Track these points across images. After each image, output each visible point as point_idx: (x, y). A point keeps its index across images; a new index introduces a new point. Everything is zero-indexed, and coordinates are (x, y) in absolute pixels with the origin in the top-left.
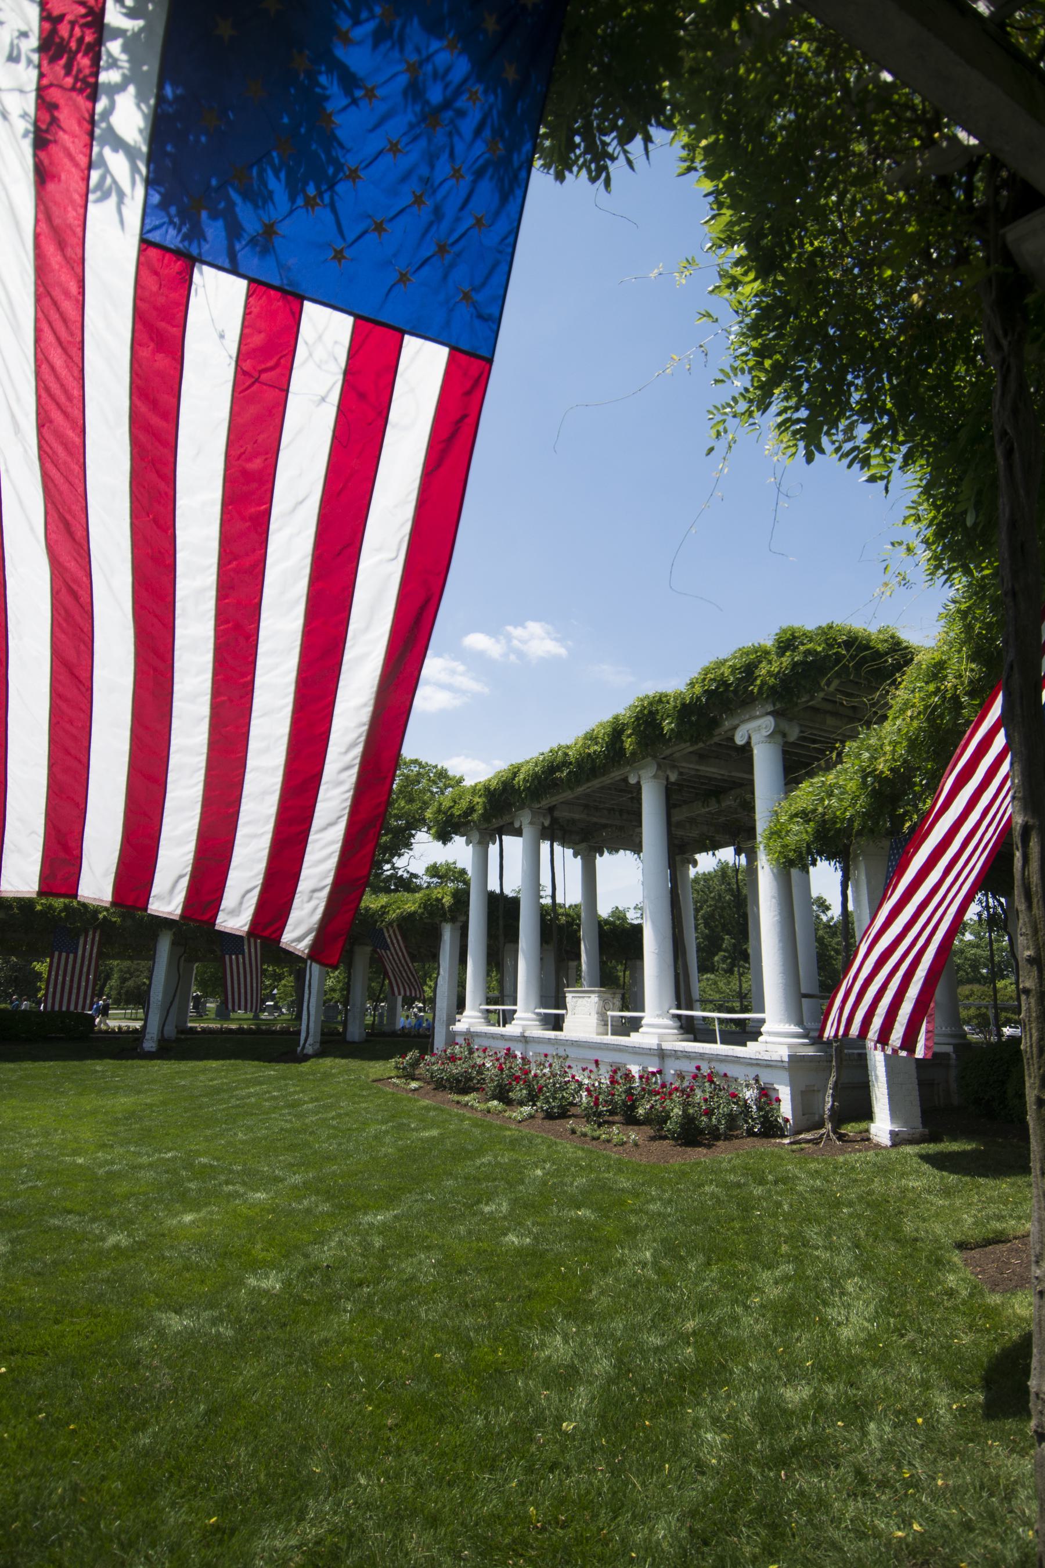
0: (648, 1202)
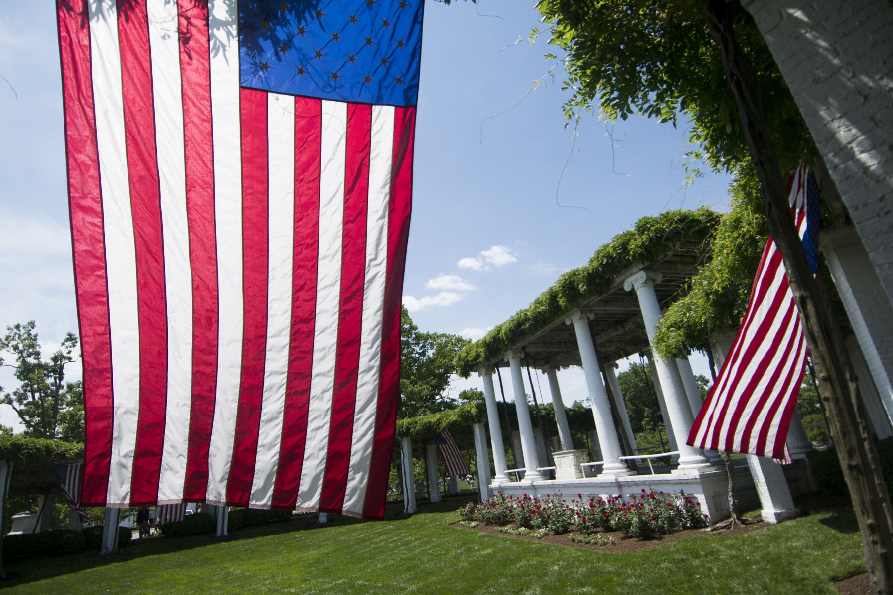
0: (626, 578)
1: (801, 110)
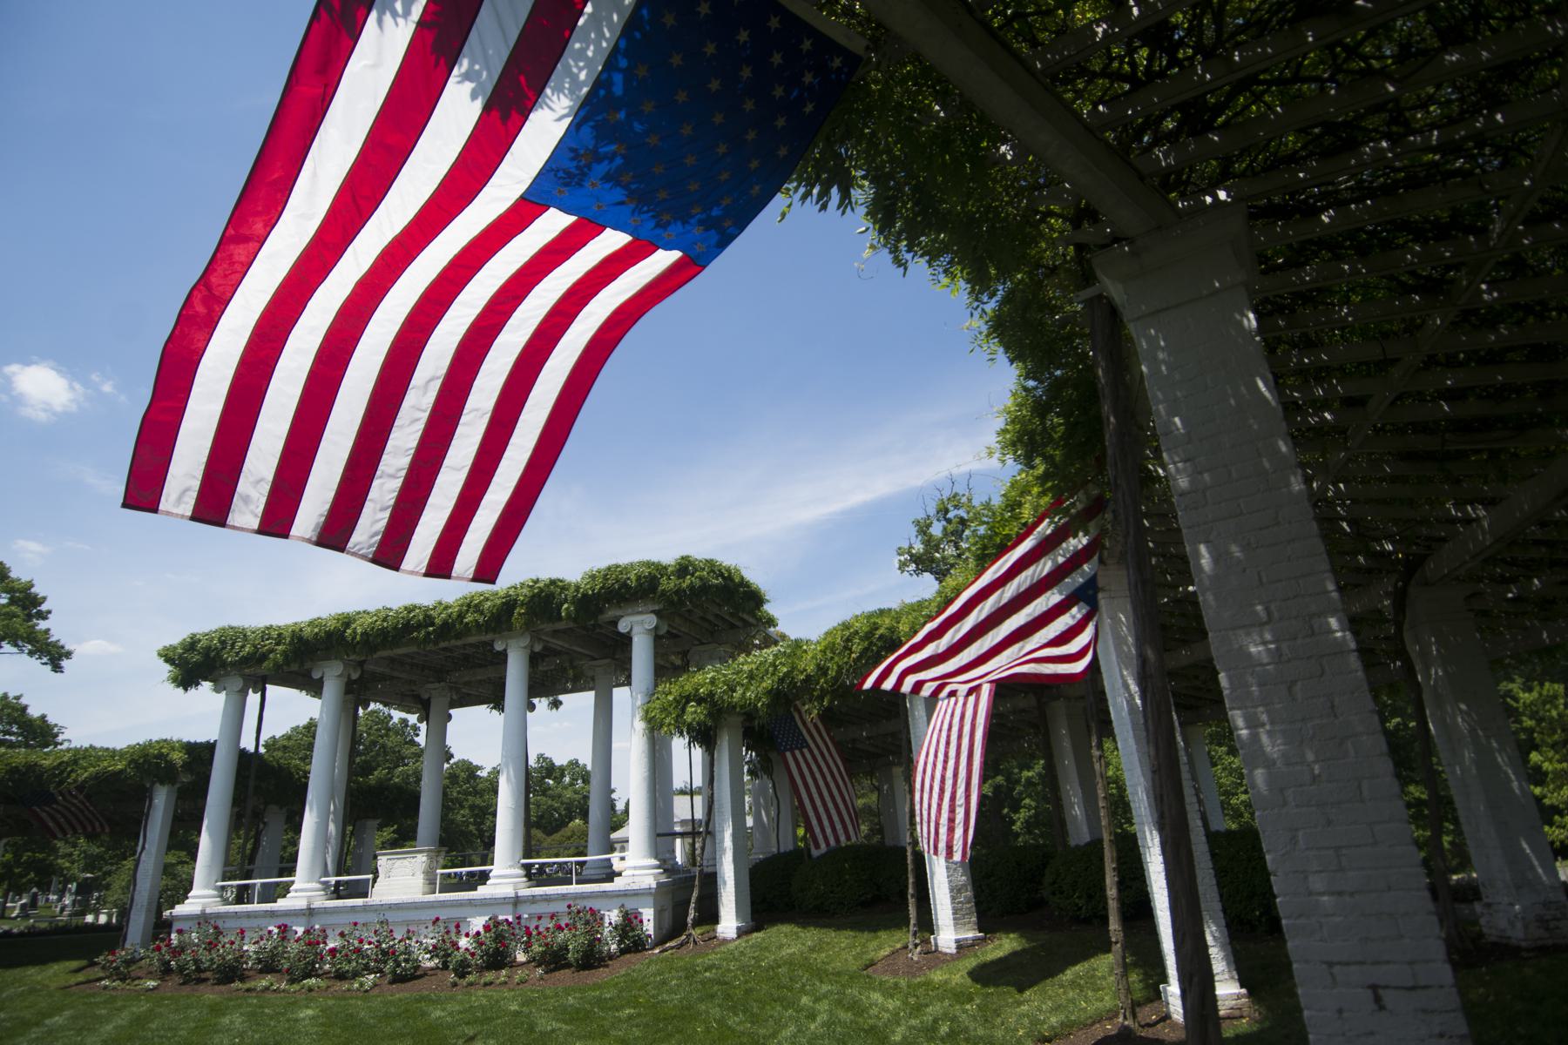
1: (1311, 1037)
